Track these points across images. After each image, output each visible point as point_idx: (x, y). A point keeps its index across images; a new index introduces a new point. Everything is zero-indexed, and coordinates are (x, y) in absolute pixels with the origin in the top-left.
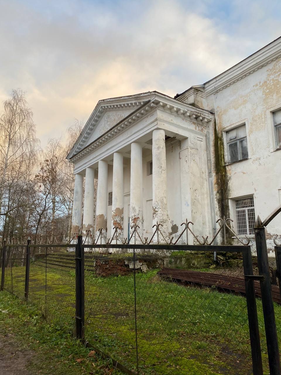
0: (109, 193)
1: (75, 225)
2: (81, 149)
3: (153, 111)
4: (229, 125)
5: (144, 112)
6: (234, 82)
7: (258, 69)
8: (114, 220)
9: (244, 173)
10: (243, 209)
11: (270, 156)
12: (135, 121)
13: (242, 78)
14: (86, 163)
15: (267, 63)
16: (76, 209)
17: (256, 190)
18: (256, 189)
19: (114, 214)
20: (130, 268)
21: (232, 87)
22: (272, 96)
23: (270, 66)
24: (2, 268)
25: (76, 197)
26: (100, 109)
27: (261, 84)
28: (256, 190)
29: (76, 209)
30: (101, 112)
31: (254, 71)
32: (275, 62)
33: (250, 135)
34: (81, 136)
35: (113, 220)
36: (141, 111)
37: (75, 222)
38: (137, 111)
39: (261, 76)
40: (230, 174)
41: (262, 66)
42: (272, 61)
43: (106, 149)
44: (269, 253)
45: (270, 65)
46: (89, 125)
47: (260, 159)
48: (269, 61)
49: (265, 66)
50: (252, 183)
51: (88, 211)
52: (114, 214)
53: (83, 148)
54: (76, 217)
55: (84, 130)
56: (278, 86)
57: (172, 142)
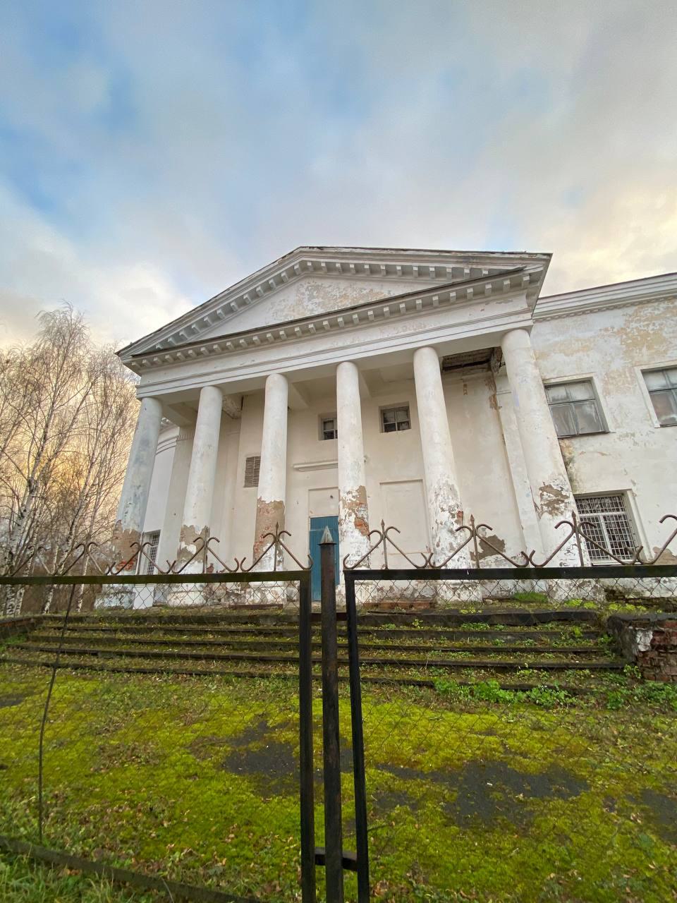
0: (249, 460)
1: (131, 528)
2: (182, 340)
3: (511, 294)
4: (555, 376)
5: (149, 364)
6: (560, 317)
7: (608, 309)
8: (356, 514)
9: (603, 454)
10: (595, 514)
11: (653, 433)
12: (212, 354)
13: (576, 314)
14: (175, 380)
15: (625, 306)
16: (140, 486)
17: (634, 484)
18: (635, 482)
19: (354, 500)
20: (298, 657)
21: (554, 322)
22: (640, 350)
23: (630, 310)
24: (588, 563)
25: (142, 453)
26: (296, 264)
27: (615, 330)
28: (634, 484)
29: (140, 486)
30: (292, 273)
31: (600, 310)
32: (636, 308)
33: (607, 397)
34: (201, 310)
35: (354, 516)
36: (176, 353)
37: (131, 519)
38: (495, 278)
39: (615, 319)
40: (570, 453)
41: (615, 307)
42: (633, 304)
43: (466, 319)
44: (8, 692)
45: (570, 318)
46: (245, 289)
47: (633, 435)
48: (661, 298)
49: (620, 308)
50: (625, 471)
51: (205, 490)
52: (354, 500)
53: (192, 339)
54: (135, 507)
55: (212, 303)
56: (649, 339)
57: (464, 377)
